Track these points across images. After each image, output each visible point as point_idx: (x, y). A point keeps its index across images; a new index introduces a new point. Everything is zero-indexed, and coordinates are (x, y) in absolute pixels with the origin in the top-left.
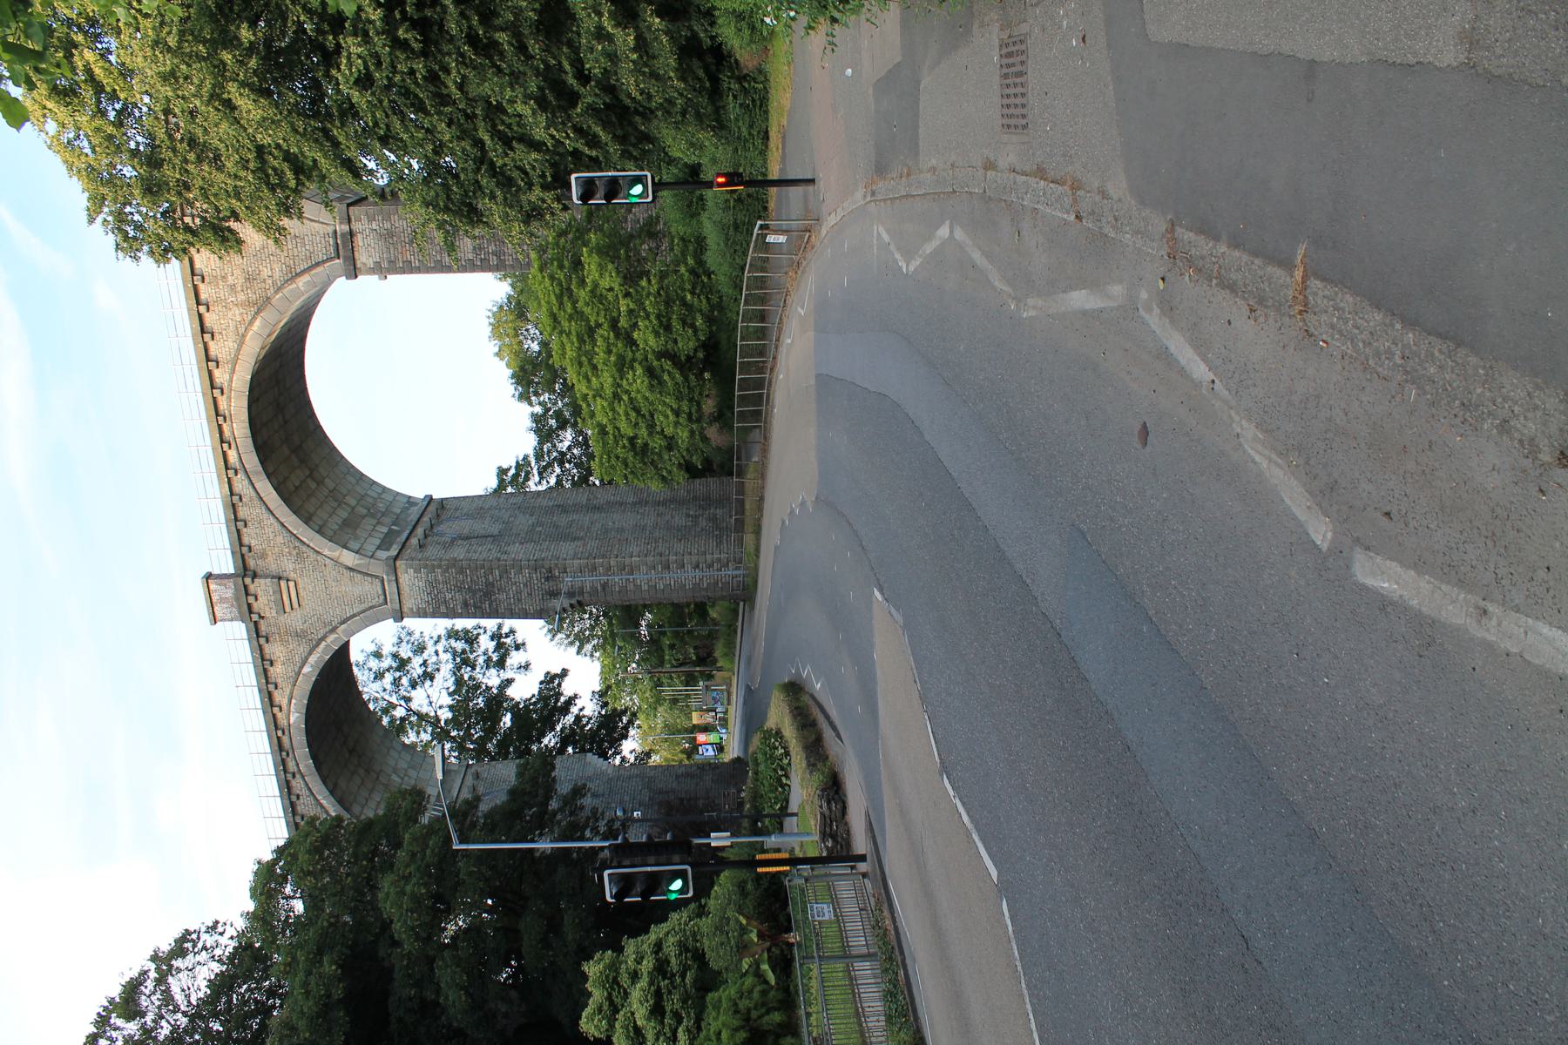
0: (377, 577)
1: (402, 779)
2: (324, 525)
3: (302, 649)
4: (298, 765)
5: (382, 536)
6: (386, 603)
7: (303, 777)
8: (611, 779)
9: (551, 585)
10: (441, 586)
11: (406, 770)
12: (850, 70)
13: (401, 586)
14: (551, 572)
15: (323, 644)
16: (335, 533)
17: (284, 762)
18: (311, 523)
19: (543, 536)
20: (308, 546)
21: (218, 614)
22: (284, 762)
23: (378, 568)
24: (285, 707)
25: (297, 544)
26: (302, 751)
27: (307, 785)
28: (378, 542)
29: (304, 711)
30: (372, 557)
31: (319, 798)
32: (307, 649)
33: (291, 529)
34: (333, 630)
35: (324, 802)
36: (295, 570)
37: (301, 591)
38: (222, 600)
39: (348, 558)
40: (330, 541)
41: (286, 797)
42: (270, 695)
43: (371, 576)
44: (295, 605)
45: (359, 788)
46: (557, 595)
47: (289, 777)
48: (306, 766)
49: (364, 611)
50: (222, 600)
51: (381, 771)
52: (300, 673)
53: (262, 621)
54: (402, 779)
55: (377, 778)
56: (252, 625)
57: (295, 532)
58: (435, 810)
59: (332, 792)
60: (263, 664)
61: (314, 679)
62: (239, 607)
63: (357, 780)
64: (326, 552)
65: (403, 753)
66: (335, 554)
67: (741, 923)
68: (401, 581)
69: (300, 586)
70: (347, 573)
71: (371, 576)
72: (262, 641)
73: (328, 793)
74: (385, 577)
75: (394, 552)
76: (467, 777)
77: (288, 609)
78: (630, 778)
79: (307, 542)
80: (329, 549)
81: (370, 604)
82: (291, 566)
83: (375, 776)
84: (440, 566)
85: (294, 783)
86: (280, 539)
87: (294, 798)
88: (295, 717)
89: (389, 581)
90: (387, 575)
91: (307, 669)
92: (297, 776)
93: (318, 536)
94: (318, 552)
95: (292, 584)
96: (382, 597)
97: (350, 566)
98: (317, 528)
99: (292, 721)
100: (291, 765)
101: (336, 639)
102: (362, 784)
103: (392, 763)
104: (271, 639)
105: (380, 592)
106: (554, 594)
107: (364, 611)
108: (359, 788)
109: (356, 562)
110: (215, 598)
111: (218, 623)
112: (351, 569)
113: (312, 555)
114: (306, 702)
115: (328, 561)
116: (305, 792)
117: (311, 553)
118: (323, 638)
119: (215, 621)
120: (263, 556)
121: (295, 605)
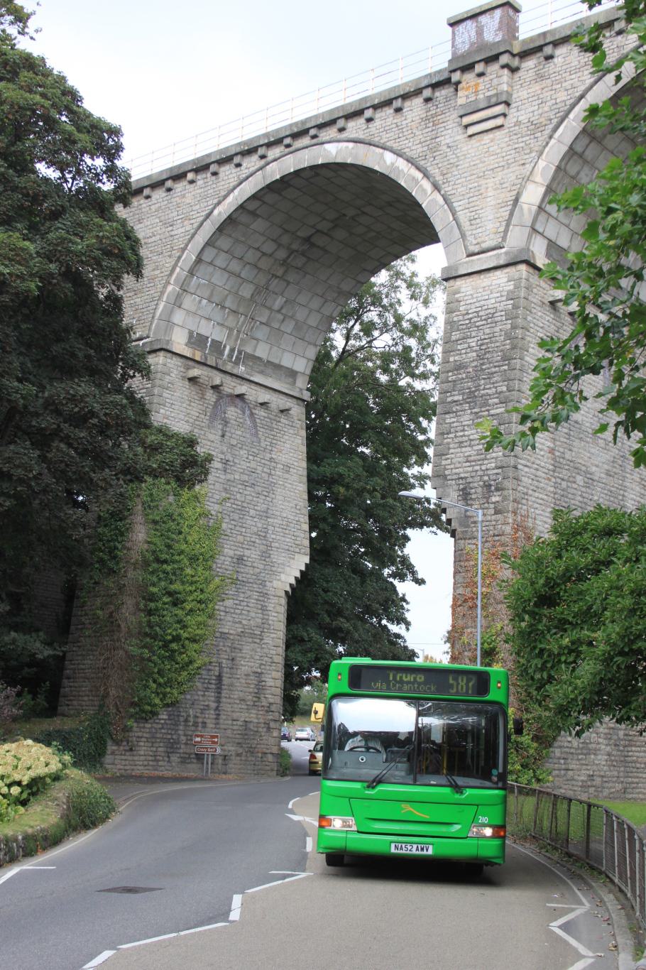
0: (504, 239)
1: (279, 311)
2: (586, 162)
3: (415, 150)
4: (275, 160)
6: (468, 256)
7: (261, 169)
8: (263, 584)
9: (476, 492)
10: (487, 331)
11: (291, 317)
13: (491, 274)
14: (497, 489)
15: (419, 175)
16: (573, 178)
17: (278, 142)
18: (586, 140)
19: (564, 484)
20: (551, 137)
21: (461, 28)
22: (278, 142)
23: (516, 239)
24: (344, 135)
25: (555, 121)
26: (283, 165)
27: (251, 175)
29: (339, 160)
30: (534, 230)
31: (236, 192)
32: (413, 154)
34: (436, 187)
36: (518, 123)
37: (487, 137)
39: (533, 195)
41: (238, 150)
42: (358, 113)
43: (506, 231)
44: (471, 130)
45: (258, 249)
46: (465, 499)
47: (261, 151)
48: (273, 172)
50: (480, 32)
51: (288, 283)
53: (452, 89)
54: (279, 311)
55: (275, 276)
56: (446, 75)
58: (232, 350)
59: (241, 207)
61: (376, 168)
62: (469, 53)
63: (269, 247)
64: (542, 164)
65: (319, 316)
66: (538, 178)
67: (387, 741)
68: (498, 273)
69: (498, 133)
70: (510, 196)
73: (240, 203)
74: (503, 250)
77: (466, 120)
79: (557, 135)
81: (468, 233)
83: (280, 273)
84: (514, 327)
85: (255, 158)
86: (562, 96)
87: (237, 160)
88: (333, 150)
89: (498, 256)
90: (506, 253)
92: (263, 162)
94: (541, 153)
95: (499, 121)
96: (476, 249)
97: (522, 199)
98: (579, 149)
99: (327, 146)
101: (424, 191)
102: (264, 254)
103: (302, 299)
104: (430, 105)
106: (465, 495)
108: (258, 249)
109: (525, 207)
110: (483, 19)
111: (450, 29)
112: (516, 200)
113: (536, 146)
114: (349, 162)
115: (529, 167)
116: (244, 171)
117: (541, 141)
118: (426, 175)
120: (540, 77)
121: (471, 130)
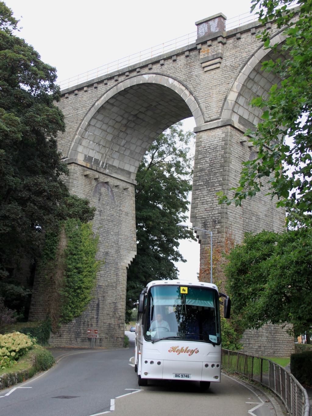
0: (220, 115)
1: (123, 146)
2: (255, 82)
3: (182, 77)
4: (122, 82)
5: (250, 120)
6: (205, 122)
7: (116, 85)
8: (117, 264)
9: (210, 223)
10: (214, 154)
11: (129, 149)
12: (23, 67)
14: (219, 223)
15: (184, 88)
18: (255, 73)
19: (247, 220)
20: (240, 72)
22: (123, 74)
24: (152, 71)
25: (242, 65)
28: (246, 116)
29: (149, 82)
31: (105, 95)
32: (181, 79)
33: (251, 60)
34: (191, 93)
35: (103, 98)
36: (226, 66)
37: (214, 71)
38: (209, 28)
39: (232, 97)
40: (243, 85)
41: (106, 77)
43: (221, 112)
44: (206, 69)
47: (116, 78)
49: (201, 110)
50: (209, 28)
51: (127, 134)
52: (169, 77)
54: (123, 146)
56: (195, 46)
57: (249, 63)
58: (103, 163)
59: (107, 102)
60: (172, 57)
61: (165, 85)
62: (204, 37)
63: (119, 119)
64: (236, 83)
68: (218, 130)
69: (217, 71)
70: (223, 97)
71: (221, 112)
72: (187, 53)
75: (237, 125)
76: (125, 183)
77: (204, 65)
78: (117, 275)
79: (242, 71)
80: (237, 85)
81: (205, 113)
82: (228, 64)
83: (124, 130)
84: (225, 153)
85: (113, 81)
86: (244, 55)
87: (105, 82)
89: (218, 123)
90: (221, 121)
91: (171, 81)
92: (116, 83)
93: (246, 77)
94: (236, 79)
95: (218, 65)
96: (209, 119)
98: (252, 77)
100: (121, 79)
101: (186, 95)
102: (117, 122)
103: (133, 141)
105: (212, 118)
107: (201, 110)
108: (114, 120)
109: (229, 102)
111: (196, 27)
112: (226, 99)
113: (234, 76)
114: (153, 82)
115: (231, 85)
116: (108, 87)
118: (187, 88)
119: (198, 24)
121: (206, 69)
